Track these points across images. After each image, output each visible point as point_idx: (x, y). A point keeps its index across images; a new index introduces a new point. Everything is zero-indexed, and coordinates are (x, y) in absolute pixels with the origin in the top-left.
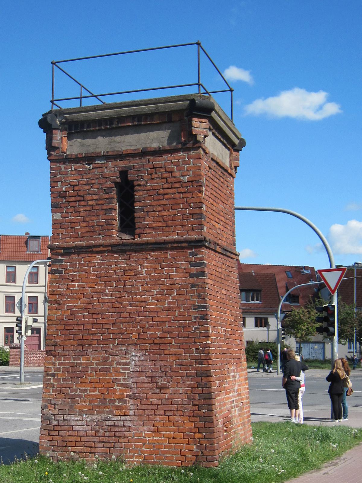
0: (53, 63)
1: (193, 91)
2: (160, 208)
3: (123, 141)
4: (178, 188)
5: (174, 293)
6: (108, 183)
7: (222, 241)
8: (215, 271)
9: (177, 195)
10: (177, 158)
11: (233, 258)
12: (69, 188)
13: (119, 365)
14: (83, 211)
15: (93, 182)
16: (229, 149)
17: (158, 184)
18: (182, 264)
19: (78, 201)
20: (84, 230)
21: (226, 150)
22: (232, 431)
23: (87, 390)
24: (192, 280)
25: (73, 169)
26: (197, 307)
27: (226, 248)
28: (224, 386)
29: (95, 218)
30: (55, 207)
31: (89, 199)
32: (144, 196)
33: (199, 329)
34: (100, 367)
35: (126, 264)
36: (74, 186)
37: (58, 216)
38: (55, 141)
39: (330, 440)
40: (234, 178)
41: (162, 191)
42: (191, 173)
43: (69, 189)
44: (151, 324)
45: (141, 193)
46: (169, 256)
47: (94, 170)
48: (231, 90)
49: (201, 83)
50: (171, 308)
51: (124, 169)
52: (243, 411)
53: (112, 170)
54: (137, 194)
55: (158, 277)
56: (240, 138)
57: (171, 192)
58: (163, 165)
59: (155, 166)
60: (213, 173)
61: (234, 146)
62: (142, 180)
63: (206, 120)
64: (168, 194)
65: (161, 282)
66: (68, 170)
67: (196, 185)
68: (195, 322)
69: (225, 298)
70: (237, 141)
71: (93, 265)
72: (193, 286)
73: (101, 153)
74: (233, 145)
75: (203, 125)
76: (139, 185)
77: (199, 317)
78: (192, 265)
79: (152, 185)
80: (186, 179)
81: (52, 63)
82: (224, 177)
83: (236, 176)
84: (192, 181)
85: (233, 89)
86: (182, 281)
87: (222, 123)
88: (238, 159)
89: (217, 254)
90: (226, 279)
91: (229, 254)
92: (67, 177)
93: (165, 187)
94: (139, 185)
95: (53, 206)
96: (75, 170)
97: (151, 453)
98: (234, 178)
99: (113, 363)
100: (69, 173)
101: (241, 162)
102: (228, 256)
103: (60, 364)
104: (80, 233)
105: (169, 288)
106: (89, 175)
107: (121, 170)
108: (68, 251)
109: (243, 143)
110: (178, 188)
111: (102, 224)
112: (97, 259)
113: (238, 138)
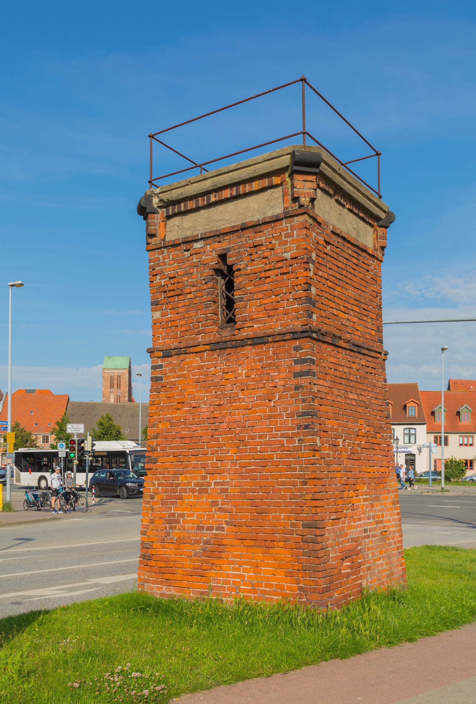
0: (151, 136)
1: (296, 143)
2: (260, 296)
3: (221, 219)
4: (280, 268)
5: (275, 398)
6: (207, 271)
7: (353, 335)
8: (335, 370)
9: (280, 277)
10: (279, 231)
11: (377, 358)
12: (168, 281)
13: (218, 486)
14: (182, 306)
15: (191, 271)
16: (372, 226)
17: (259, 266)
18: (285, 362)
19: (177, 295)
20: (183, 329)
21: (368, 227)
22: (362, 567)
23: (184, 514)
24: (295, 381)
25: (171, 259)
26: (301, 414)
27: (360, 343)
28: (345, 511)
29: (194, 314)
30: (155, 304)
31: (187, 292)
32: (244, 282)
33: (303, 441)
34: (197, 488)
35: (226, 365)
36: (172, 278)
37: (157, 315)
38: (151, 227)
39: (122, 606)
40: (381, 261)
41: (263, 274)
42: (295, 248)
43: (168, 283)
44: (251, 436)
45: (241, 279)
46: (271, 353)
47: (191, 258)
48: (378, 154)
49: (307, 130)
50: (271, 417)
51: (223, 252)
52: (387, 542)
53: (209, 253)
54: (237, 281)
55: (258, 379)
56: (387, 211)
57: (273, 274)
58: (264, 242)
59: (255, 244)
60: (335, 250)
61: (378, 220)
62: (241, 263)
63: (313, 178)
64: (269, 277)
65: (262, 385)
66: (166, 261)
67: (301, 262)
68: (299, 433)
69: (355, 404)
70: (383, 215)
71: (191, 369)
72: (297, 388)
73: (198, 236)
74: (377, 219)
75: (309, 185)
76: (239, 270)
77: (304, 426)
78: (296, 362)
79: (253, 267)
80: (288, 255)
81: (149, 136)
82: (360, 258)
83: (384, 259)
84: (296, 258)
85: (381, 152)
86: (285, 383)
87: (352, 189)
88: (384, 238)
89: (340, 350)
90: (359, 381)
91: (373, 354)
92: (166, 269)
93: (267, 269)
94: (239, 270)
95: (152, 304)
96: (173, 259)
97: (249, 591)
98: (381, 261)
99: (211, 483)
100: (167, 264)
101: (389, 243)
102: (364, 354)
103: (159, 485)
104: (179, 332)
105: (271, 392)
106: (188, 263)
107: (220, 253)
108: (167, 354)
109: (390, 218)
110: (280, 268)
111: (200, 320)
112: (195, 361)
113: (385, 212)
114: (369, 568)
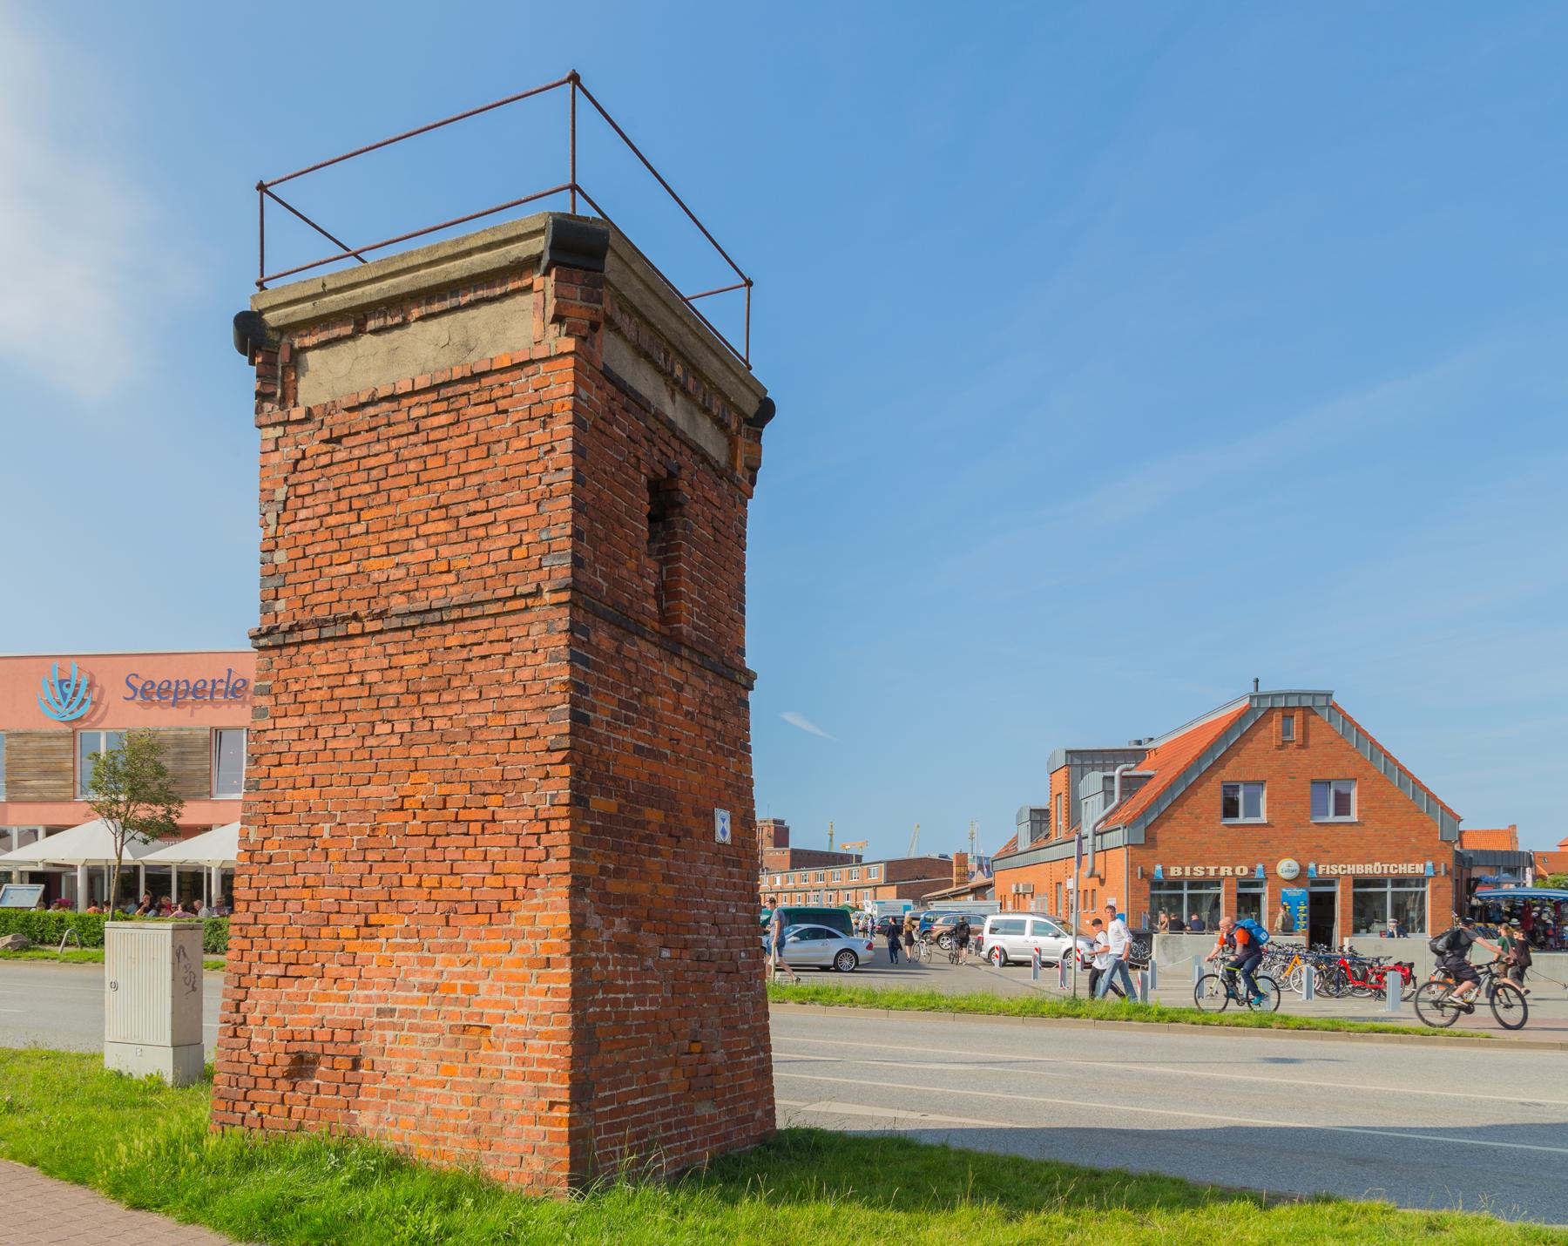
114: (386, 1094)
